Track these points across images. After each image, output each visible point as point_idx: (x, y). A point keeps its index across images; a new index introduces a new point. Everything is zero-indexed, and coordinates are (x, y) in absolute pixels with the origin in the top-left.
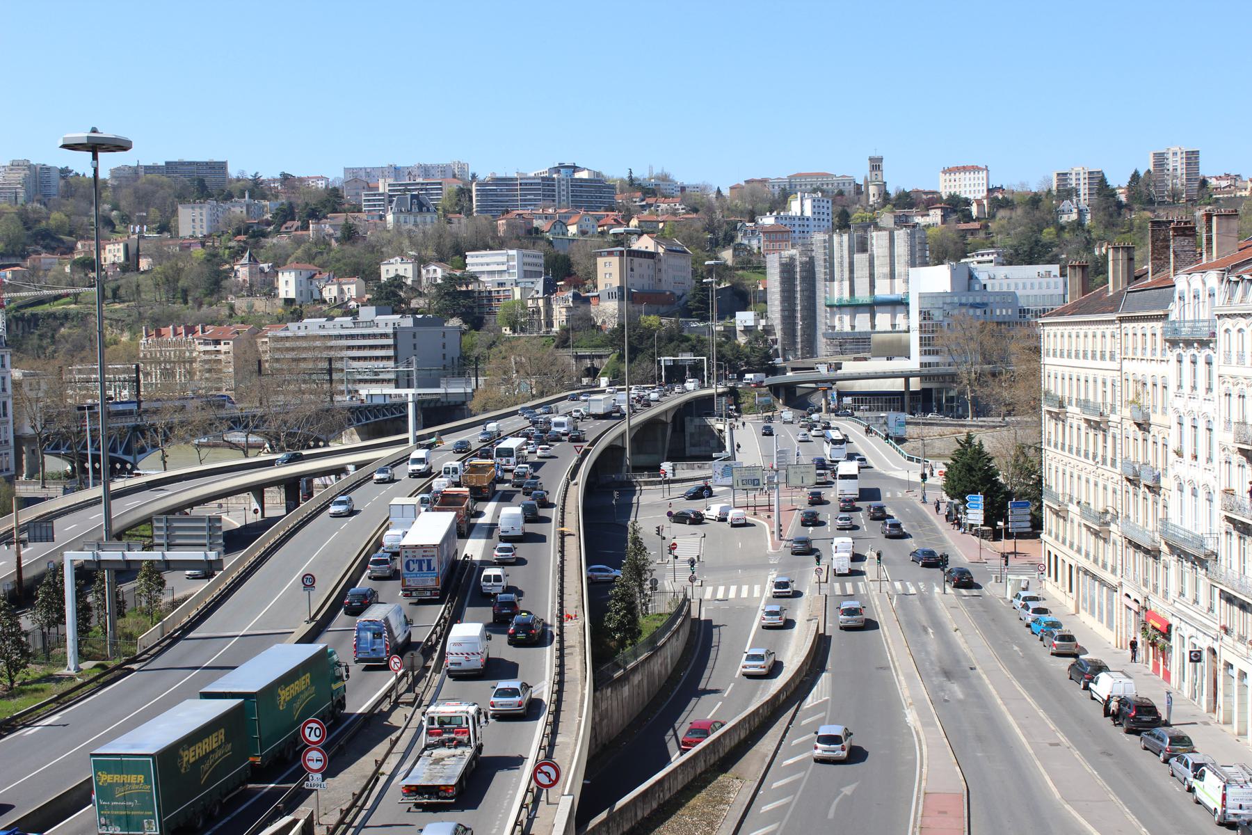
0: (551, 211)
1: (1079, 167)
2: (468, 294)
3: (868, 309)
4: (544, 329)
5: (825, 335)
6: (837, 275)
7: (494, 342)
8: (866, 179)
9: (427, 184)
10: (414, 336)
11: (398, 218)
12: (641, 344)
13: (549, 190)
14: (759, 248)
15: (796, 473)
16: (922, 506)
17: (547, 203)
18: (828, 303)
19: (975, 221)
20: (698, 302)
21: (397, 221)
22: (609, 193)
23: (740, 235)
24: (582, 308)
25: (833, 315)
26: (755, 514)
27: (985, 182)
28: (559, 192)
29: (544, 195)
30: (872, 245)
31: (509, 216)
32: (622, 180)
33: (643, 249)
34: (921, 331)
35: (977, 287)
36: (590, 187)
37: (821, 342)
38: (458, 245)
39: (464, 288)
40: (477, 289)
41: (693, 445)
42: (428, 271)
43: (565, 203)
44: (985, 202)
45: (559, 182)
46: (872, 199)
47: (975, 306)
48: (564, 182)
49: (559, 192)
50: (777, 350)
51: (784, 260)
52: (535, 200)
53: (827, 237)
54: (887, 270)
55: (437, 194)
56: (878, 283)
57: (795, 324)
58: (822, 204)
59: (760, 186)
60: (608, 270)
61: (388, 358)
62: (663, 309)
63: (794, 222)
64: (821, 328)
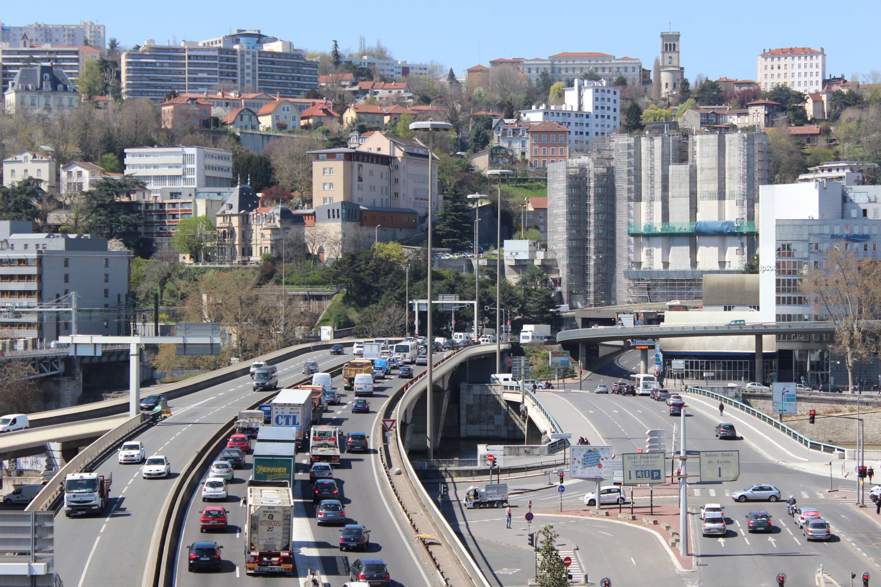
0: (232, 95)
1: (87, 20)
2: (131, 207)
3: (687, 240)
4: (239, 258)
5: (627, 274)
6: (645, 193)
7: (169, 275)
8: (657, 61)
9: (57, 52)
10: (66, 264)
11: (23, 98)
12: (377, 281)
13: (228, 67)
14: (523, 154)
15: (710, 462)
16: (861, 512)
17: (226, 85)
18: (633, 231)
19: (810, 122)
20: (449, 225)
21: (21, 103)
22: (310, 72)
23: (496, 136)
24: (294, 229)
25: (638, 247)
26: (634, 518)
27: (820, 70)
28: (242, 70)
29: (221, 73)
30: (694, 153)
31: (177, 100)
32: (324, 56)
33: (374, 151)
34: (778, 272)
35: (854, 213)
36: (285, 63)
37: (623, 286)
38: (110, 139)
39: (125, 199)
40: (143, 201)
41: (470, 422)
42: (70, 174)
43: (250, 85)
44: (824, 98)
45: (242, 56)
46: (664, 90)
47: (852, 238)
48: (250, 57)
49: (242, 70)
50: (560, 293)
51: (572, 172)
52: (209, 80)
53: (632, 140)
54: (714, 187)
55: (71, 67)
56: (701, 204)
57: (586, 258)
58: (607, 96)
59: (510, 68)
60: (328, 178)
61: (28, 293)
62: (402, 234)
63: (568, 120)
64: (622, 265)
